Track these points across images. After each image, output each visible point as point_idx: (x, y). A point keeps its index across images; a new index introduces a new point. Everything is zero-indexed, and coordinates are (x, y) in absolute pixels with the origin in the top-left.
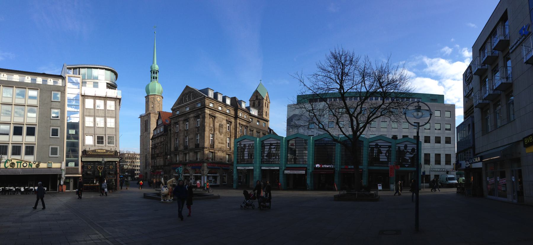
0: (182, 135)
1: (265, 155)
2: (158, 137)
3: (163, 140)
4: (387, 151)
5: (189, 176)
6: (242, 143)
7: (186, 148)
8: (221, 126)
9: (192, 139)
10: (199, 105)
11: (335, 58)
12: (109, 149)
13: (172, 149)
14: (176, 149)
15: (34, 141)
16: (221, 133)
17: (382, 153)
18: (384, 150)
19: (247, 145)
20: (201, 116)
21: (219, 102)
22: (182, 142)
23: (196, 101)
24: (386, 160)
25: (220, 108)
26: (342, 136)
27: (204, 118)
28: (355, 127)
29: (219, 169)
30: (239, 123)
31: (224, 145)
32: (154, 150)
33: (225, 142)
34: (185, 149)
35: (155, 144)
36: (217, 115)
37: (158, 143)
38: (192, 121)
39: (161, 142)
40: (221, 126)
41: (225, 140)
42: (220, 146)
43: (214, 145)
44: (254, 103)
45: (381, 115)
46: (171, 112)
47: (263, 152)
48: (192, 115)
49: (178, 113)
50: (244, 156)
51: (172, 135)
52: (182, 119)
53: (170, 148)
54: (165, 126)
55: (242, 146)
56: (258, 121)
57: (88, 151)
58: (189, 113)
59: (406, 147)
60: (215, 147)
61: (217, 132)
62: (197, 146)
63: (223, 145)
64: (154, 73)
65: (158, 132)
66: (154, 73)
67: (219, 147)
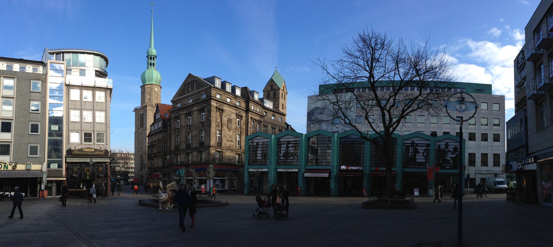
0: (183, 131)
1: (282, 155)
2: (156, 134)
3: (161, 138)
4: (425, 150)
5: (192, 180)
6: (254, 141)
7: (188, 146)
8: (230, 121)
9: (196, 136)
10: (204, 96)
11: (364, 41)
13: (173, 148)
14: (177, 148)
16: (229, 129)
17: (418, 153)
18: (421, 149)
19: (260, 143)
20: (206, 110)
22: (183, 139)
24: (424, 161)
25: (228, 100)
27: (210, 111)
28: (387, 122)
30: (251, 118)
31: (233, 144)
33: (234, 140)
34: (200, 146)
35: (152, 143)
36: (226, 108)
37: (156, 141)
38: (195, 115)
39: (160, 140)
40: (230, 121)
41: (234, 137)
42: (228, 144)
43: (221, 143)
44: (269, 94)
45: (418, 108)
46: (171, 104)
47: (279, 151)
48: (195, 108)
49: (179, 105)
50: (256, 156)
51: (172, 131)
53: (170, 146)
55: (255, 144)
56: (274, 116)
58: (192, 106)
59: (447, 145)
61: (225, 128)
62: (202, 144)
63: (232, 143)
64: (151, 59)
65: (156, 128)
66: (151, 59)
67: (228, 145)
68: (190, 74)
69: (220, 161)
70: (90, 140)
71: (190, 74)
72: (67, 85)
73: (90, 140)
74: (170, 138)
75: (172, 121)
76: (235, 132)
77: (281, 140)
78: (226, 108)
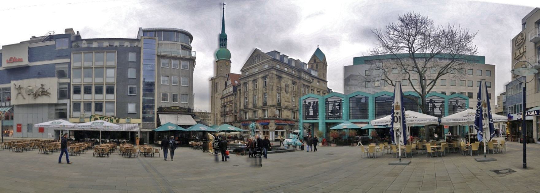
1: (330, 111)
4: (441, 105)
7: (255, 106)
8: (287, 86)
11: (402, 20)
12: (183, 106)
13: (242, 107)
14: (246, 107)
15: (91, 98)
16: (287, 92)
17: (436, 108)
18: (438, 105)
21: (285, 64)
23: (263, 63)
24: (440, 114)
25: (286, 69)
26: (534, 81)
28: (432, 84)
29: (286, 125)
32: (223, 109)
33: (291, 101)
34: (263, 105)
35: (224, 103)
36: (283, 76)
37: (227, 102)
39: (230, 101)
41: (290, 98)
42: (286, 104)
43: (280, 103)
44: (312, 66)
45: (447, 72)
46: (241, 73)
47: (327, 109)
49: (247, 73)
50: (309, 113)
51: (242, 94)
52: (252, 79)
53: (240, 106)
54: (234, 86)
55: (307, 103)
56: (319, 82)
57: (164, 108)
59: (457, 101)
60: (282, 105)
67: (286, 105)
68: (484, 57)
69: (279, 117)
70: (101, 110)
71: (484, 57)
72: (158, 56)
73: (101, 110)
74: (240, 99)
75: (242, 86)
76: (291, 94)
77: (329, 100)
78: (283, 76)
